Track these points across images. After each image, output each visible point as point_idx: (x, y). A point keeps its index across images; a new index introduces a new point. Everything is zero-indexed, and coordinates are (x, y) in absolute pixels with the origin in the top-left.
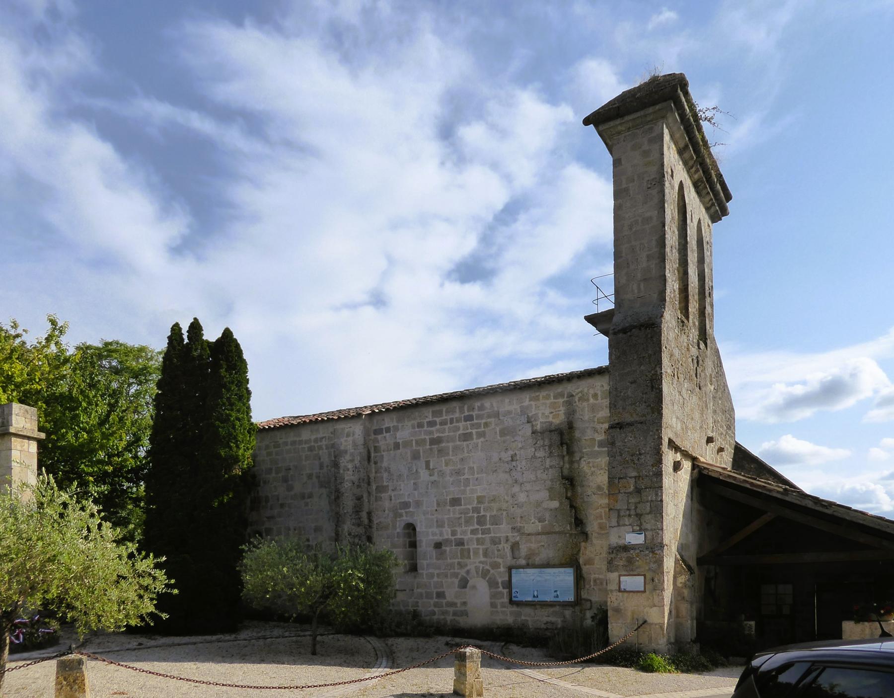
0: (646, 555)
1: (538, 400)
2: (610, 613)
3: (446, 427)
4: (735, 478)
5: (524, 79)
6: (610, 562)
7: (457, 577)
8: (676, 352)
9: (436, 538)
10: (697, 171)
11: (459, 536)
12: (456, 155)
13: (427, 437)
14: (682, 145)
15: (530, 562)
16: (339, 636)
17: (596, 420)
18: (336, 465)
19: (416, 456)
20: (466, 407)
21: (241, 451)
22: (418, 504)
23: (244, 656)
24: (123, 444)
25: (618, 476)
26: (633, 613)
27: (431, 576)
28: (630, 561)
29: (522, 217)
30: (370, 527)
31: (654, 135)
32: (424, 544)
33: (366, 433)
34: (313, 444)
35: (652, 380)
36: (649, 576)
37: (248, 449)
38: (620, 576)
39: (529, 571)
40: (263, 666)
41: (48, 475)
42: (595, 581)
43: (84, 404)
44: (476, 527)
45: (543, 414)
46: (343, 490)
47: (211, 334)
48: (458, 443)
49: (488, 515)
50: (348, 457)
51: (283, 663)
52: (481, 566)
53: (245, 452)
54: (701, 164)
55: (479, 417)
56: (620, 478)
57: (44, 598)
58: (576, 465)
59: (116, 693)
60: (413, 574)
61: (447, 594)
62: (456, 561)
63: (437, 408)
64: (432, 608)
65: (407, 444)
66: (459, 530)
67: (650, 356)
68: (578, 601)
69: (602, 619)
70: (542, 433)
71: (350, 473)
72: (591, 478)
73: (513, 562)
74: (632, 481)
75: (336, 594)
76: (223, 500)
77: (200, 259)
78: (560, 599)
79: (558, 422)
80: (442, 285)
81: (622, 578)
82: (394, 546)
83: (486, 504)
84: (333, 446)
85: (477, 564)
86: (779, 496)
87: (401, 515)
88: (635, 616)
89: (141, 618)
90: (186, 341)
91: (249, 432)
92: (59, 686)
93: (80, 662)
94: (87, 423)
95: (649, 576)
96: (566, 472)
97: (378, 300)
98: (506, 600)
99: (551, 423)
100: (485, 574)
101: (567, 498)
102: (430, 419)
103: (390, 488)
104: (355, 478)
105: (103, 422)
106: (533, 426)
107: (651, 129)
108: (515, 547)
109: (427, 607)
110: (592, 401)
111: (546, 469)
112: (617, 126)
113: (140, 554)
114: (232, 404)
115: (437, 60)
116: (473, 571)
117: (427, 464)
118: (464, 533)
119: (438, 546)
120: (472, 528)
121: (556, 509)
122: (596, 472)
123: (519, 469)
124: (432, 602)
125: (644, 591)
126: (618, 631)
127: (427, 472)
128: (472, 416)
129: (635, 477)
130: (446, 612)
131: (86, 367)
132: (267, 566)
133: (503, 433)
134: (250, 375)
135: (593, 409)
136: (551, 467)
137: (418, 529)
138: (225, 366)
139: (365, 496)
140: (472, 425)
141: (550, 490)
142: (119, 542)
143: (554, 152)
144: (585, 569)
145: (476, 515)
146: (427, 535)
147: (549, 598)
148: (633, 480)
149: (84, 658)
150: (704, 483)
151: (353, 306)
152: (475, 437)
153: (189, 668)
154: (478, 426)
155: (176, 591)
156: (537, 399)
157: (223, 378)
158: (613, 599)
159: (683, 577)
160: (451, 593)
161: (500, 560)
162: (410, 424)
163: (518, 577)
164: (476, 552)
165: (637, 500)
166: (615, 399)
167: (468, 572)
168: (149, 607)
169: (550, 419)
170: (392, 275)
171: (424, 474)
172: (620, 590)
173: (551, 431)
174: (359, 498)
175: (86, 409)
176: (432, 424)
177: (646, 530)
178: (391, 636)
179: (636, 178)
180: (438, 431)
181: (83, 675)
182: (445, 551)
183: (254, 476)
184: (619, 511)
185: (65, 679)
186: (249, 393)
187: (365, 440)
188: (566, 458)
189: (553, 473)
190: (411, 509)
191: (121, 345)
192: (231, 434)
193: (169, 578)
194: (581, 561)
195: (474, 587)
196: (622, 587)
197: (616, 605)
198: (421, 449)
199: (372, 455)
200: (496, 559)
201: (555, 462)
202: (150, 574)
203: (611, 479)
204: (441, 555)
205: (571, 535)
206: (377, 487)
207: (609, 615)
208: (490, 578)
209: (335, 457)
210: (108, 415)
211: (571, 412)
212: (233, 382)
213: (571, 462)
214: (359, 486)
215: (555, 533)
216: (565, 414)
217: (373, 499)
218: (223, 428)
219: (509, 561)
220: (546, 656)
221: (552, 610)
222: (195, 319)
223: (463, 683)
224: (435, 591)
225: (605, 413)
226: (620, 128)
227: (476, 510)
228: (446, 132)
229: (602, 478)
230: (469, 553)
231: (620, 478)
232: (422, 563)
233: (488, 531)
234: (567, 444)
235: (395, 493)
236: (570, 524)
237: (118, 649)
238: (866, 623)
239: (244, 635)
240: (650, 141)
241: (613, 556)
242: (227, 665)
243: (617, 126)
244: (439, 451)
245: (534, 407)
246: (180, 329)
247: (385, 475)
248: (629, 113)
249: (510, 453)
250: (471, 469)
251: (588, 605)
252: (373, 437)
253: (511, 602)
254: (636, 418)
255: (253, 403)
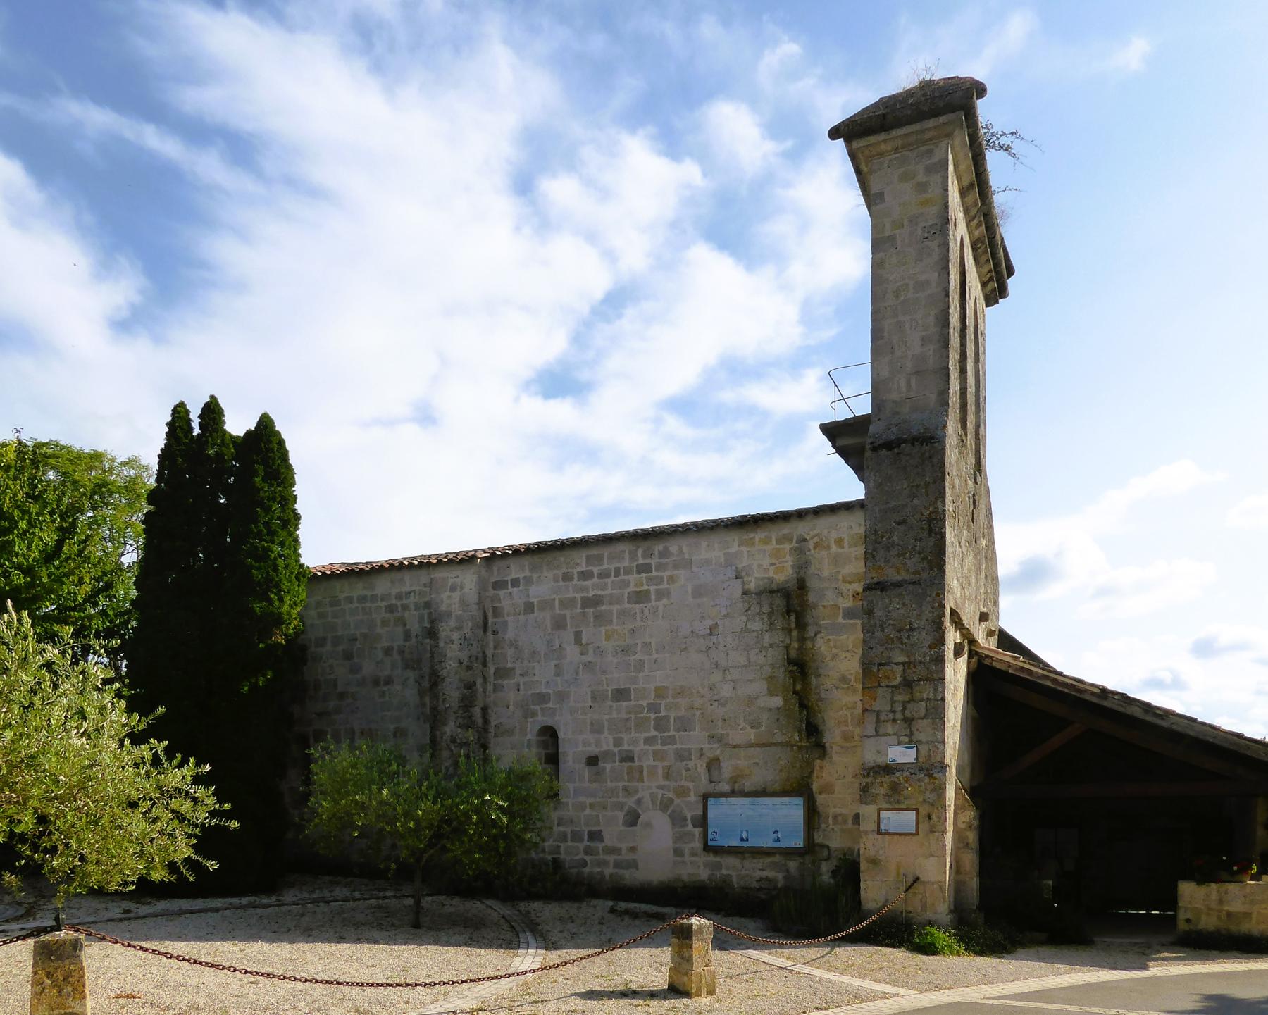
0: (919, 780)
1: (753, 544)
2: (863, 866)
3: (609, 581)
4: (1030, 672)
5: (634, 118)
6: (865, 789)
7: (621, 809)
8: (957, 482)
9: (589, 749)
10: (979, 225)
11: (626, 747)
12: (541, 221)
13: (578, 596)
14: (966, 183)
15: (737, 787)
16: (442, 898)
17: (840, 577)
18: (432, 633)
19: (559, 624)
20: (640, 552)
21: (286, 607)
22: (562, 697)
23: (310, 932)
24: (86, 589)
25: (877, 660)
26: (898, 867)
27: (582, 807)
28: (895, 788)
29: (630, 312)
30: (486, 730)
31: (935, 159)
32: (570, 758)
33: (482, 586)
34: (394, 602)
35: (930, 521)
36: (923, 811)
37: (295, 603)
38: (879, 810)
39: (733, 800)
40: (346, 947)
41: (17, 611)
42: (835, 817)
43: (23, 524)
44: (653, 733)
45: (760, 566)
46: (444, 673)
47: (238, 424)
48: (627, 606)
50: (452, 623)
51: (376, 942)
52: (660, 792)
53: (293, 607)
54: (985, 215)
55: (660, 567)
56: (880, 665)
57: (11, 831)
58: (809, 644)
59: (119, 996)
61: (606, 835)
62: (621, 784)
63: (594, 551)
64: (581, 856)
65: (546, 605)
66: (626, 737)
67: (927, 484)
68: (810, 848)
69: (850, 871)
70: (759, 594)
71: (455, 646)
72: (831, 664)
73: (711, 788)
74: (899, 669)
75: (465, 832)
76: (257, 682)
77: (158, 340)
78: (784, 844)
79: (782, 578)
80: (517, 399)
81: (883, 814)
84: (427, 605)
85: (654, 790)
86: (1094, 700)
87: (534, 714)
88: (902, 871)
89: (172, 867)
90: (197, 431)
91: (298, 579)
92: (38, 989)
93: (76, 946)
94: (25, 557)
95: (923, 811)
96: (793, 654)
97: (425, 416)
98: (698, 844)
99: (772, 580)
100: (665, 805)
101: (795, 692)
102: (583, 567)
103: (518, 672)
104: (464, 656)
105: (50, 556)
106: (743, 583)
107: (930, 152)
108: (713, 764)
109: (572, 853)
110: (834, 548)
111: (762, 649)
112: (879, 143)
113: (170, 758)
114: (272, 533)
115: (509, 83)
116: (647, 800)
117: (578, 636)
118: (634, 742)
119: (592, 761)
120: (647, 735)
121: (778, 709)
122: (840, 654)
123: (721, 647)
124: (581, 846)
125: (917, 833)
126: (875, 892)
127: (577, 649)
128: (649, 565)
129: (904, 664)
130: (605, 863)
131: (23, 467)
132: (350, 782)
133: (698, 592)
134: (298, 490)
135: (836, 560)
136: (771, 646)
137: (561, 735)
138: (262, 473)
139: (479, 681)
140: (650, 579)
141: (770, 679)
142: (138, 739)
143: (674, 225)
144: (820, 799)
145: (652, 716)
147: (766, 842)
148: (900, 668)
149: (82, 936)
150: (983, 677)
151: (390, 423)
152: (653, 597)
153: (226, 950)
154: (659, 580)
155: (234, 824)
156: (751, 543)
157: (258, 490)
158: (869, 845)
159: (967, 813)
161: (690, 785)
162: (550, 575)
163: (717, 810)
164: (653, 771)
165: (906, 698)
166: (874, 545)
167: (639, 802)
168: (183, 850)
169: (771, 574)
170: (506, 357)
171: (572, 652)
172: (879, 832)
173: (771, 592)
174: (470, 686)
175: (25, 532)
176: (585, 575)
177: (918, 742)
178: (523, 899)
179: (906, 223)
180: (595, 587)
181: (82, 968)
182: (604, 769)
183: (304, 648)
184: (878, 713)
185: (49, 975)
186: (297, 517)
187: (480, 598)
188: (795, 633)
189: (776, 655)
190: (550, 705)
191: (63, 447)
192: (272, 580)
193: (221, 801)
194: (815, 787)
195: (648, 825)
196: (882, 827)
197: (872, 853)
198: (568, 613)
199: (490, 620)
200: (683, 783)
201: (778, 637)
202: (187, 793)
203: (866, 665)
204: (598, 776)
205: (800, 748)
206: (497, 670)
207: (862, 868)
209: (432, 622)
210: (60, 544)
211: (802, 565)
212: (274, 499)
213: (802, 639)
214: (469, 668)
215: (775, 744)
216: (793, 567)
217: (490, 688)
218: (258, 569)
219: (704, 784)
220: (768, 930)
221: (769, 860)
222: (212, 397)
223: (686, 974)
224: (586, 830)
225: (856, 566)
226: (883, 147)
227: (653, 708)
228: (523, 185)
229: (850, 665)
230: (641, 772)
231: (880, 665)
233: (672, 740)
234: (795, 611)
235: (526, 679)
236: (800, 732)
237: (91, 919)
238: (1213, 885)
239: (289, 896)
240: (929, 170)
241: (869, 780)
242: (288, 947)
243: (879, 143)
244: (596, 617)
245: (745, 554)
246: (187, 412)
247: (510, 652)
248: (899, 124)
249: (709, 622)
250: (646, 644)
251: (825, 853)
252: (491, 592)
253: (707, 848)
254: (904, 576)
255: (302, 533)
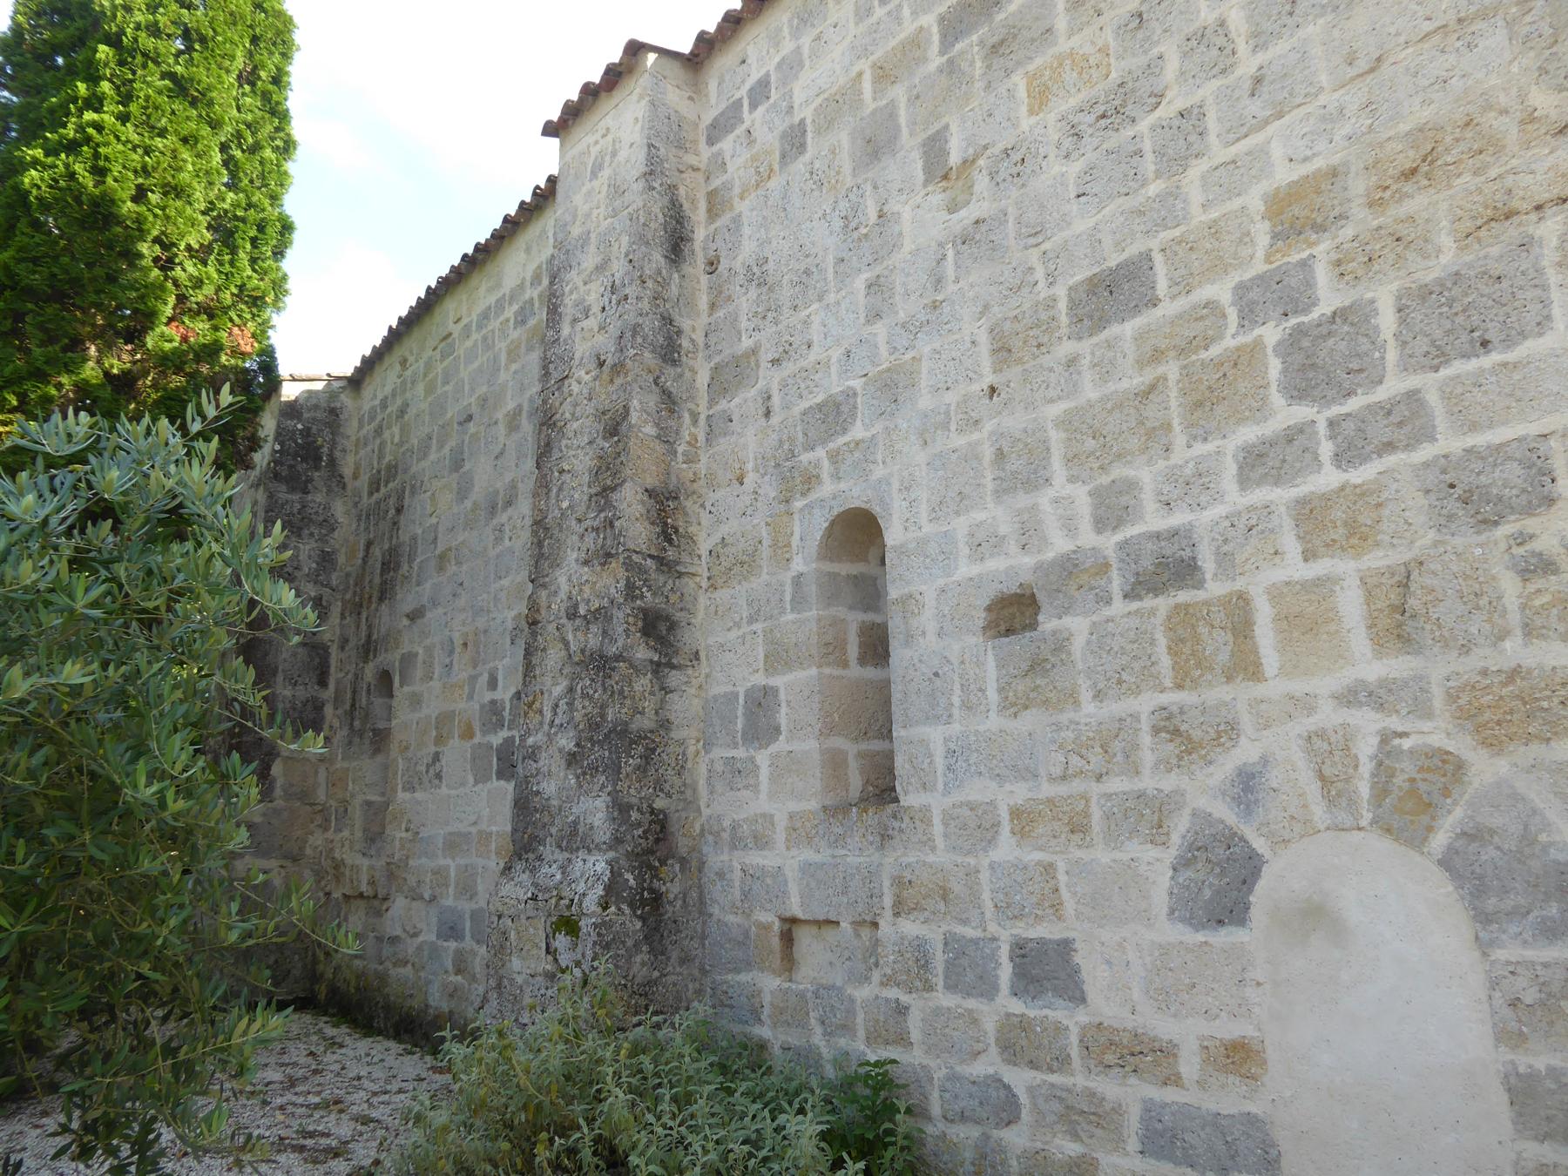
7: (1158, 834)
9: (995, 564)
11: (1154, 520)
27: (978, 828)
32: (927, 620)
44: (1285, 413)
49: (1384, 297)
52: (1368, 725)
60: (871, 817)
62: (1145, 704)
66: (1146, 475)
82: (777, 659)
83: (1361, 220)
85: (1328, 716)
87: (811, 480)
100: (1410, 799)
116: (1294, 775)
119: (1014, 613)
120: (1249, 434)
137: (893, 535)
146: (941, 570)
160: (1130, 958)
164: (1307, 617)
167: (1247, 787)
182: (1061, 644)
190: (858, 432)
195: (1314, 917)
204: (1037, 683)
208: (1473, 835)
224: (1006, 935)
227: (1281, 292)
232: (923, 741)
233: (1408, 420)
235: (789, 368)
